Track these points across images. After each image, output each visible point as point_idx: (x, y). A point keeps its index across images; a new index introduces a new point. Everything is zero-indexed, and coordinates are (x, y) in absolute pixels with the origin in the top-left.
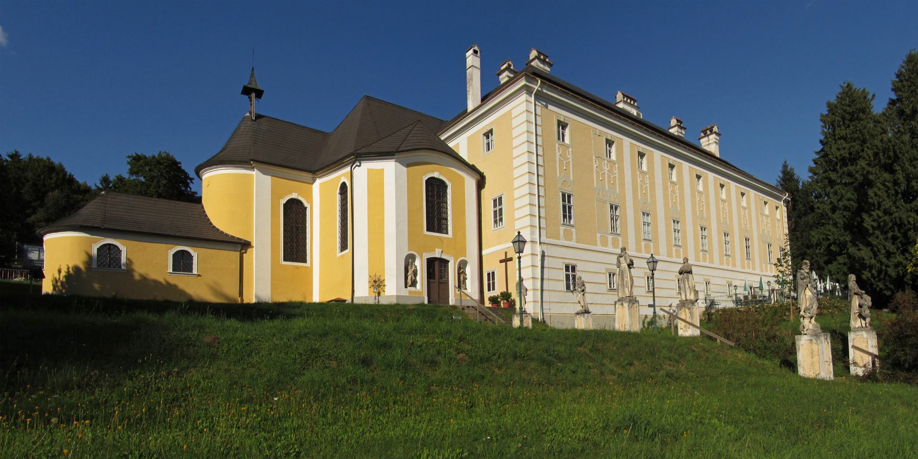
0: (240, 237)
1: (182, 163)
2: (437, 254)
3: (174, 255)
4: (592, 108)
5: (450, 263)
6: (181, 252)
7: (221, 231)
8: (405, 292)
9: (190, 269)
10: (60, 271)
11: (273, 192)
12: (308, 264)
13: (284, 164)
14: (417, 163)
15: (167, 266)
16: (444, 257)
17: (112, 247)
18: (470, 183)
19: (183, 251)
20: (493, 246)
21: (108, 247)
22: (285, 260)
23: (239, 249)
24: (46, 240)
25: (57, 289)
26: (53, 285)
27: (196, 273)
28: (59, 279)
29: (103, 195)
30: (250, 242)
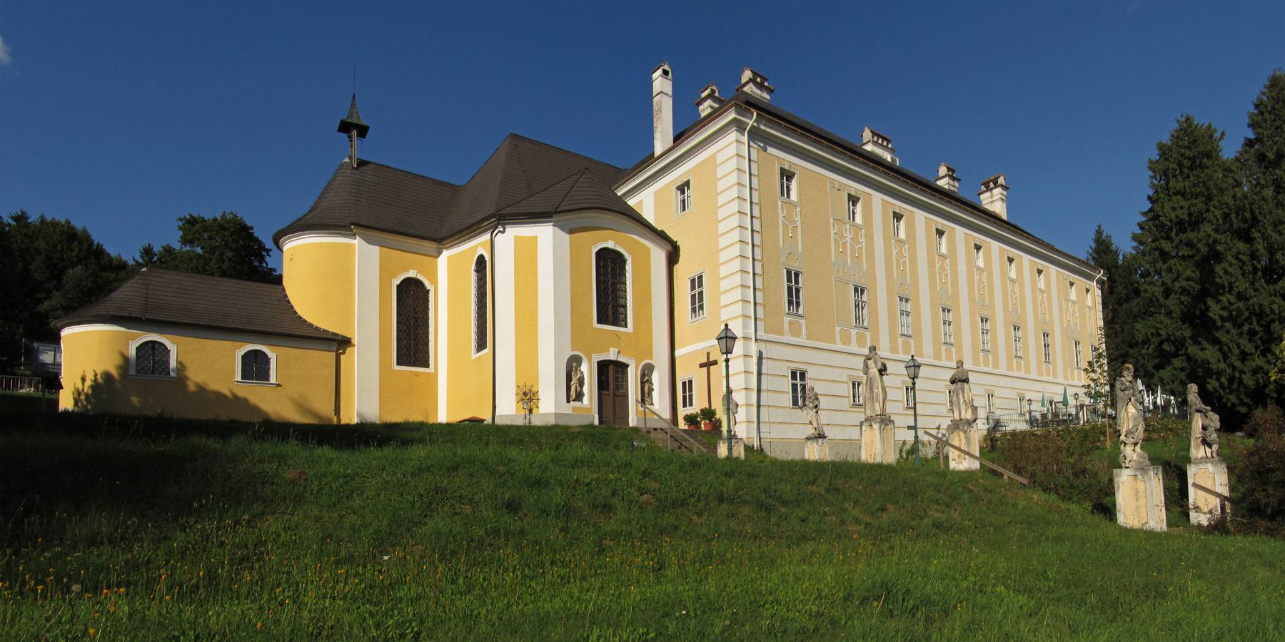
0: (336, 332)
1: (255, 228)
2: (612, 355)
3: (243, 357)
4: (829, 150)
5: (629, 368)
6: (253, 353)
7: (310, 323)
8: (567, 409)
9: (266, 376)
10: (83, 380)
11: (382, 269)
12: (431, 369)
13: (397, 229)
14: (584, 227)
15: (234, 372)
16: (621, 359)
17: (157, 346)
18: (658, 256)
19: (256, 351)
20: (690, 344)
21: (151, 345)
22: (399, 363)
23: (335, 349)
24: (65, 336)
25: (80, 404)
26: (74, 398)
27: (275, 382)
28: (83, 390)
29: (144, 273)
30: (350, 339)
